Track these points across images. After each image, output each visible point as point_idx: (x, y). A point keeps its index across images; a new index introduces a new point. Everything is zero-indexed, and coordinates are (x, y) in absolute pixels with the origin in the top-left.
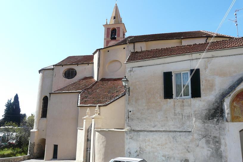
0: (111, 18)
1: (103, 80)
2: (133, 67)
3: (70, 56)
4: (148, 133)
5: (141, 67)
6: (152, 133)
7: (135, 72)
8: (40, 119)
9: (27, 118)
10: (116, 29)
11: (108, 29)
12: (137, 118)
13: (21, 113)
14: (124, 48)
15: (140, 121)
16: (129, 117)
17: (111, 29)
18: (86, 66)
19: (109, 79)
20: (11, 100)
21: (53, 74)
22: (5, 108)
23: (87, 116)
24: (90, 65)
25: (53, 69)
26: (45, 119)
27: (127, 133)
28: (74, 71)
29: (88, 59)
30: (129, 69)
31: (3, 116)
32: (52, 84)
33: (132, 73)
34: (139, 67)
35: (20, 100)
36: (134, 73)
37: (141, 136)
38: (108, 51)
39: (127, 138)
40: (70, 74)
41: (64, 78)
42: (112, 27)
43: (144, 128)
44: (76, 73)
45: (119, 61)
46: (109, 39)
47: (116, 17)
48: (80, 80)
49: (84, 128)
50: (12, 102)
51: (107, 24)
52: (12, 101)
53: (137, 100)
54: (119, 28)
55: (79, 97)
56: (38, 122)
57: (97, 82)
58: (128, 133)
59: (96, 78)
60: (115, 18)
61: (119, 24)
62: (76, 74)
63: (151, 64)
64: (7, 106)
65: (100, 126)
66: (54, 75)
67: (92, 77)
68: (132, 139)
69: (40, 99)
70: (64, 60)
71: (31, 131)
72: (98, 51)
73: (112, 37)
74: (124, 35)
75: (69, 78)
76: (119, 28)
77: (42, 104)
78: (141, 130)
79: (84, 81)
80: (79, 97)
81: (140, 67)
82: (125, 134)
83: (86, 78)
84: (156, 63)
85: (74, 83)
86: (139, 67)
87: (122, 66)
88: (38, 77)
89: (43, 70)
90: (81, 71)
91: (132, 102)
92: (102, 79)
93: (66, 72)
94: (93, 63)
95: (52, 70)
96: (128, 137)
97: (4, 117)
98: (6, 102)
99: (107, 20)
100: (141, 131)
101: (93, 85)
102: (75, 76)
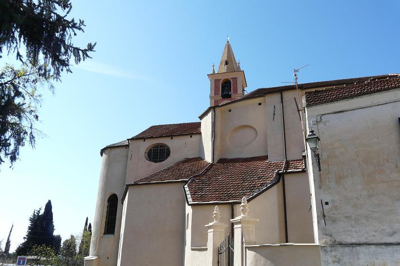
0: (221, 63)
1: (222, 161)
2: (323, 115)
3: (154, 125)
4: (379, 249)
5: (341, 112)
6: (390, 248)
7: (327, 124)
8: (101, 236)
9: (62, 242)
10: (231, 81)
11: (217, 81)
12: (346, 217)
13: (55, 233)
14: (260, 104)
15: (353, 223)
16: (325, 214)
17: (221, 81)
18: (187, 139)
19: (235, 159)
20: (40, 211)
21: (128, 155)
22: (29, 224)
23: (215, 221)
24: (195, 137)
25: (127, 146)
26: (111, 236)
27: (325, 250)
28: (166, 148)
29: (193, 129)
30: (315, 119)
31: (25, 238)
32: (126, 172)
33: (321, 125)
34: (335, 113)
35: (54, 210)
36: (326, 125)
37: (361, 256)
38: (230, 111)
39: (327, 262)
40: (158, 154)
41: (148, 161)
42: (223, 78)
43: (366, 238)
44: (169, 152)
45: (253, 128)
46: (219, 97)
47: (229, 61)
48: (178, 164)
49: (210, 245)
50: (40, 214)
51: (214, 73)
52: (42, 212)
53: (339, 179)
54: (235, 79)
55: (187, 189)
56: (98, 243)
57: (212, 165)
58: (329, 249)
59: (208, 158)
60: (227, 63)
61: (235, 73)
62: (168, 154)
63: (362, 105)
64: (32, 222)
65: (253, 238)
66: (130, 156)
67: (200, 159)
68: (338, 262)
69: (102, 200)
70: (144, 131)
71: (86, 258)
72: (212, 110)
73: (225, 93)
74: (244, 90)
75: (156, 162)
76: (235, 79)
77: (106, 210)
78: (358, 242)
79: (186, 165)
80: (187, 189)
81: (339, 112)
82: (322, 253)
83: (187, 161)
84: (375, 102)
85: (169, 169)
86: (335, 113)
87: (258, 137)
88: (99, 163)
89: (109, 149)
90: (179, 148)
91: (328, 183)
92: (220, 159)
93: (151, 150)
94: (200, 133)
95: (142, 141)
96: (330, 260)
97: (26, 239)
98: (31, 215)
99: (213, 66)
100: (360, 244)
101: (207, 170)
102: (166, 158)
